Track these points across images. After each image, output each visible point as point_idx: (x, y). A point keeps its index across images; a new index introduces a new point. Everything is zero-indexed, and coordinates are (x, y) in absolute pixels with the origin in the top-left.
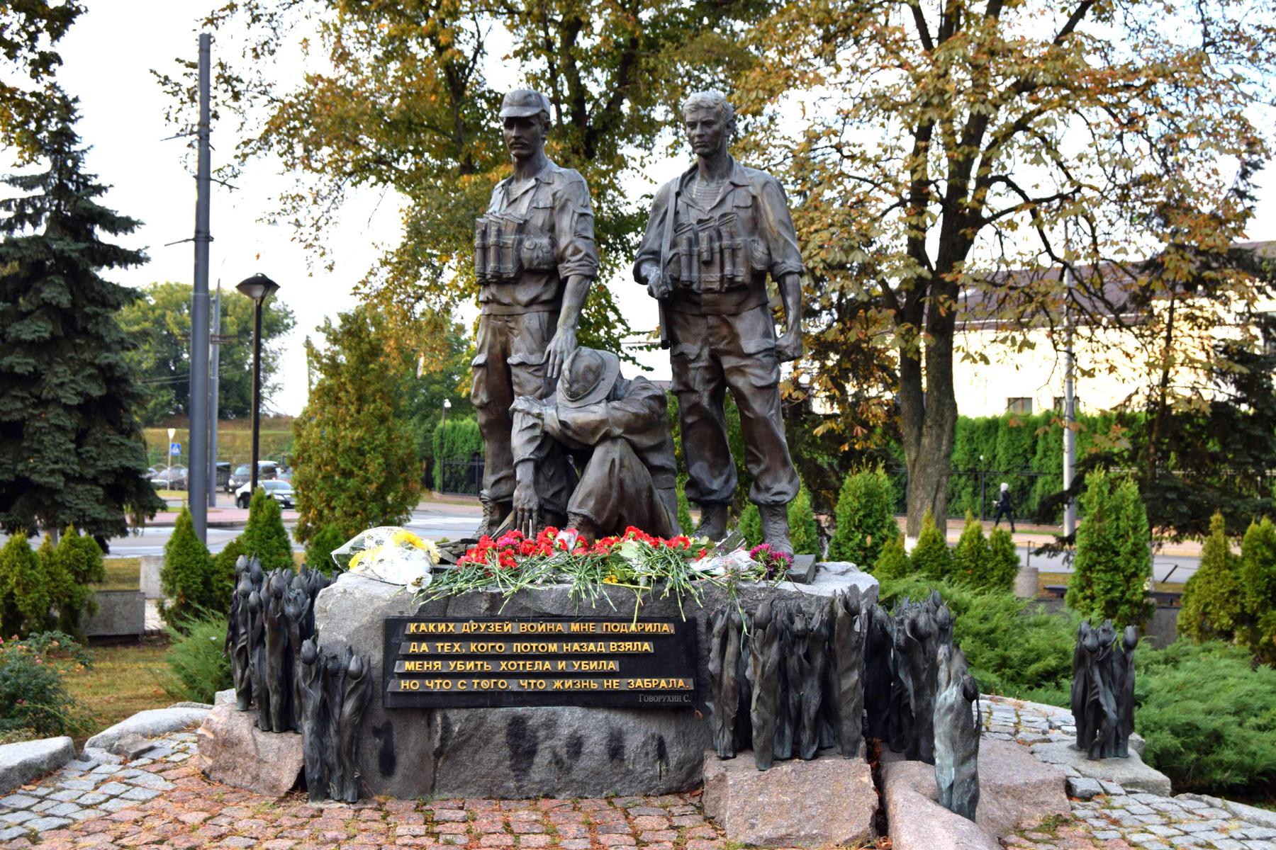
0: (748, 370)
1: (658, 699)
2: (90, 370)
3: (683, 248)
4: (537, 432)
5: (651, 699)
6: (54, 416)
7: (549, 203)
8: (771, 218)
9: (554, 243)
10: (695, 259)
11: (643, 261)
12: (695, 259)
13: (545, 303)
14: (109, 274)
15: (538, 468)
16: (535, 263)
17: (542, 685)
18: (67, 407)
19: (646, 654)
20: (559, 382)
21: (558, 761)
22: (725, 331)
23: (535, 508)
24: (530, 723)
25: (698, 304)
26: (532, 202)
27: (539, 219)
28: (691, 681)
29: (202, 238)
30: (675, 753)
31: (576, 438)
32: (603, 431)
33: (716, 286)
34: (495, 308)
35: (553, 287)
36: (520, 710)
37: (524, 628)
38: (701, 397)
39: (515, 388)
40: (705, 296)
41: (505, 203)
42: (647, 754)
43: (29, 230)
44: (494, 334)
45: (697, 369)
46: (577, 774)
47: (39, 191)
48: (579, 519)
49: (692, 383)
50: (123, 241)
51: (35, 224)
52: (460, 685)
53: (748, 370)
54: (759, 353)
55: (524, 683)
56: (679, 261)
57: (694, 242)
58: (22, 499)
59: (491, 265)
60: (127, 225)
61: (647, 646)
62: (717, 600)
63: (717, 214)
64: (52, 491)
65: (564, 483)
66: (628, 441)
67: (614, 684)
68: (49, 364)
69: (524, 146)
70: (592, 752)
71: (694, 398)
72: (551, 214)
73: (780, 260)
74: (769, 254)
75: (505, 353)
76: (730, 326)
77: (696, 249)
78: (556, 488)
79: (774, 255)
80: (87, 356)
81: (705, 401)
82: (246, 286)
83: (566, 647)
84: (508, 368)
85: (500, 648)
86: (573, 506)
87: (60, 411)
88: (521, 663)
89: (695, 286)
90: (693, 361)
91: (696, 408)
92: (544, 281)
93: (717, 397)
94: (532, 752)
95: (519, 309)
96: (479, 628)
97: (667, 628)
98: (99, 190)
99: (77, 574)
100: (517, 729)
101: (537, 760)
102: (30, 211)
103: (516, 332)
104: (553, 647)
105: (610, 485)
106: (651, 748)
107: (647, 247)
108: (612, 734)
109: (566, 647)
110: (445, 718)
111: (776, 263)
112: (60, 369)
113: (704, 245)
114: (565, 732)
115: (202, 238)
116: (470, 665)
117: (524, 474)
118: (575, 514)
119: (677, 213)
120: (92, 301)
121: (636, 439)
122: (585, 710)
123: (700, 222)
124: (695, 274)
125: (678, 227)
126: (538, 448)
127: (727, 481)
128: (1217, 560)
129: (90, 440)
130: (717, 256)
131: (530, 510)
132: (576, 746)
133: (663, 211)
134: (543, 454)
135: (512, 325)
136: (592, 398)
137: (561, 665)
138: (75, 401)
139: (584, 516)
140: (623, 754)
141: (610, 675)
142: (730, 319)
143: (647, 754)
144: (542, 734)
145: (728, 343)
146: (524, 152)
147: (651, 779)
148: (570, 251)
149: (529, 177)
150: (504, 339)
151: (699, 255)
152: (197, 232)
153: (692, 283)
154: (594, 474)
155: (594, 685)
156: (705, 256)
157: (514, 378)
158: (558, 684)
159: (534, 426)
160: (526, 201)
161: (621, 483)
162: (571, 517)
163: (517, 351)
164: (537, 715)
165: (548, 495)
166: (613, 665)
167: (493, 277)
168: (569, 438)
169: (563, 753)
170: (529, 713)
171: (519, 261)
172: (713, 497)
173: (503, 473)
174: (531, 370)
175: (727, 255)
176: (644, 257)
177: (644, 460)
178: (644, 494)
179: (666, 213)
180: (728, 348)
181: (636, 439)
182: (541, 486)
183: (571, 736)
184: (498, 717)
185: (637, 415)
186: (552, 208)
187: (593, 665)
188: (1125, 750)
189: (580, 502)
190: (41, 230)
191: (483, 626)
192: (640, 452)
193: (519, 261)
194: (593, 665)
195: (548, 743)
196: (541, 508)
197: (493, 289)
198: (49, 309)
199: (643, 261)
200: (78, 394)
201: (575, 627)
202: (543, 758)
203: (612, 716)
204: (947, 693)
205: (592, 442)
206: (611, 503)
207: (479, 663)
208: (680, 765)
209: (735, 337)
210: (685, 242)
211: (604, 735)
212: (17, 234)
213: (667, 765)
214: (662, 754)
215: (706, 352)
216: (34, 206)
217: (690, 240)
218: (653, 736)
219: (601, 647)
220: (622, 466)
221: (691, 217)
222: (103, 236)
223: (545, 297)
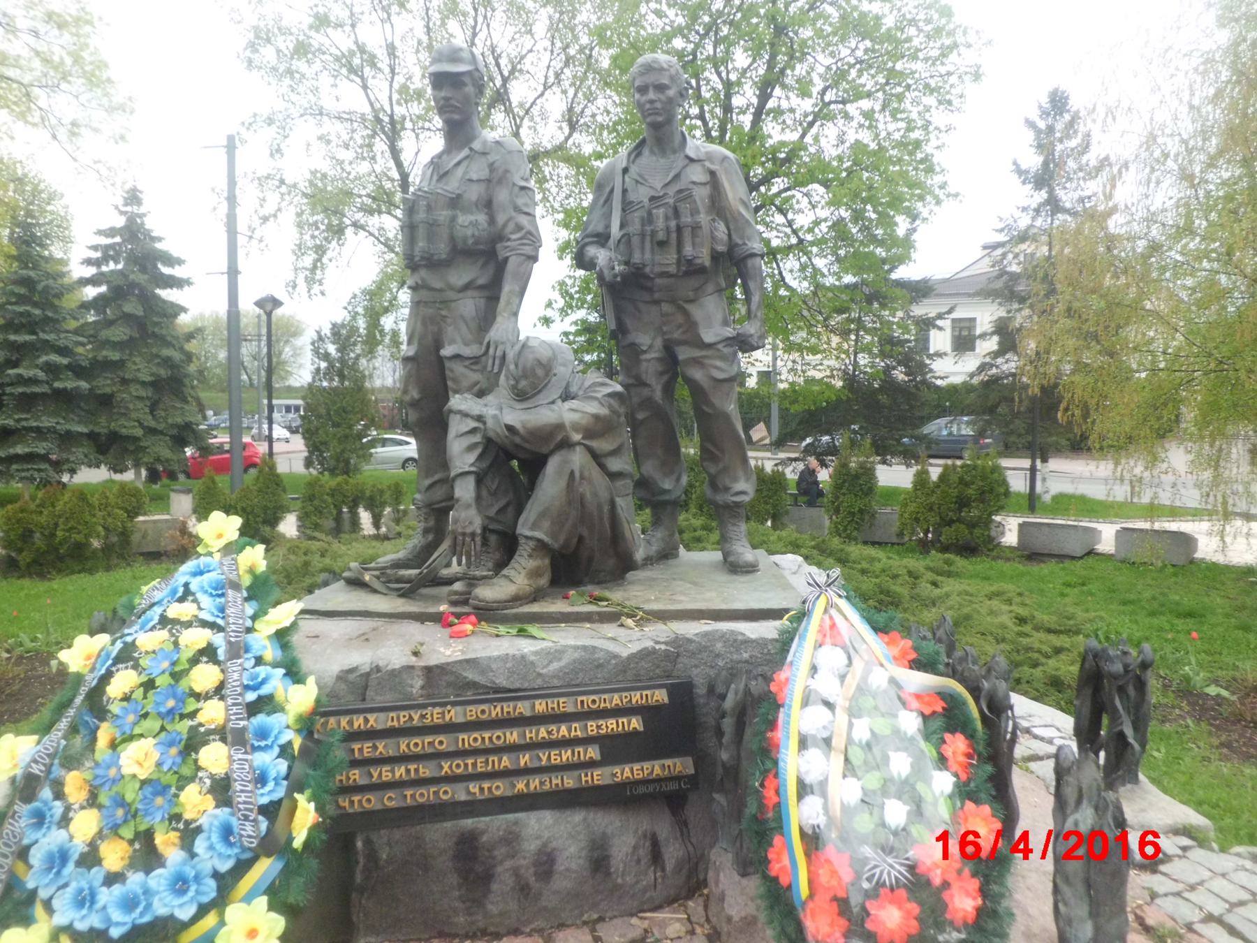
0: (707, 361)
1: (651, 788)
2: (157, 361)
3: (635, 227)
4: (477, 438)
5: (642, 790)
6: (135, 390)
7: (484, 174)
8: (730, 195)
9: (492, 221)
10: (648, 239)
11: (586, 244)
12: (648, 239)
13: (481, 287)
14: (166, 294)
15: (480, 481)
16: (470, 242)
17: (500, 788)
18: (143, 383)
19: (635, 732)
20: (502, 377)
21: (523, 889)
22: (680, 318)
23: (479, 531)
24: (485, 838)
25: (650, 290)
26: (465, 173)
27: (474, 193)
28: (689, 761)
29: (233, 273)
30: (673, 853)
31: (527, 446)
32: (559, 438)
33: (672, 269)
34: (425, 294)
35: (490, 270)
36: (469, 823)
37: (473, 713)
38: (653, 391)
39: (450, 383)
40: (658, 281)
41: (435, 178)
42: (639, 861)
43: (112, 266)
44: (424, 323)
45: (649, 361)
46: (549, 900)
47: (118, 239)
48: (532, 543)
49: (644, 377)
50: (177, 272)
51: (116, 262)
52: (390, 800)
53: (707, 361)
54: (719, 342)
55: (474, 787)
56: (629, 242)
57: (649, 219)
58: (114, 447)
59: (421, 244)
60: (179, 262)
61: (635, 723)
62: (718, 656)
63: (672, 191)
64: (136, 439)
65: (511, 496)
66: (585, 445)
67: (599, 777)
68: (131, 354)
69: (455, 109)
70: (567, 870)
71: (646, 392)
72: (488, 188)
73: (740, 242)
74: (729, 235)
75: (438, 344)
76: (686, 313)
77: (648, 228)
78: (502, 503)
79: (734, 237)
80: (154, 350)
81: (658, 395)
82: (259, 304)
83: (530, 734)
84: (441, 360)
85: (443, 742)
86: (523, 529)
87: (138, 386)
88: (470, 761)
89: (647, 270)
90: (645, 352)
91: (648, 403)
92: (480, 263)
93: (668, 389)
94: (486, 878)
95: (451, 295)
96: (411, 718)
97: (661, 696)
98: (160, 239)
99: (127, 511)
100: (468, 847)
101: (495, 887)
102: (111, 253)
103: (449, 320)
104: (513, 736)
105: (569, 503)
106: (644, 852)
107: (590, 230)
108: (593, 842)
109: (530, 734)
110: (368, 842)
111: (737, 245)
112: (138, 360)
113: (660, 223)
114: (531, 846)
115: (233, 273)
116: (400, 772)
117: (465, 490)
118: (527, 537)
119: (625, 191)
120: (158, 314)
121: (594, 444)
122: (557, 814)
123: (652, 199)
124: (648, 256)
125: (627, 206)
126: (480, 457)
127: (678, 479)
128: (921, 480)
129: (161, 406)
130: (674, 236)
131: (473, 535)
132: (546, 863)
133: (608, 189)
134: (484, 465)
135: (444, 313)
136: (543, 398)
137: (525, 759)
138: (149, 379)
139: (539, 540)
140: (608, 867)
141: (592, 764)
142: (687, 306)
143: (639, 861)
144: (500, 852)
145: (684, 333)
146: (456, 117)
147: (645, 890)
148: (511, 226)
149: (461, 148)
150: (435, 329)
151: (653, 233)
152: (229, 268)
153: (645, 266)
154: (550, 487)
155: (569, 782)
156: (661, 236)
157: (447, 372)
158: (520, 786)
159: (473, 431)
160: (460, 172)
161: (582, 497)
162: (522, 541)
163: (453, 342)
164: (492, 825)
165: (492, 512)
166: (593, 752)
167: (422, 258)
168: (517, 446)
169: (529, 875)
170: (482, 826)
171: (452, 239)
172: (667, 497)
173: (437, 477)
174: (467, 363)
175: (687, 233)
176: (587, 240)
177: (602, 466)
178: (606, 508)
179: (612, 191)
180: (684, 337)
181: (594, 444)
182: (484, 503)
183: (540, 852)
184: (440, 834)
185: (596, 417)
186: (489, 181)
187: (567, 755)
188: (1137, 776)
189: (531, 526)
190: (120, 266)
191: (416, 717)
192: (596, 456)
193: (452, 239)
194: (567, 755)
195: (508, 864)
196: (485, 529)
197: (423, 273)
198: (127, 317)
199: (586, 244)
200: (152, 375)
201: (540, 706)
202: (503, 882)
203: (592, 815)
204: (1077, 816)
205: (545, 450)
206: (570, 522)
207: (412, 767)
208: (678, 868)
209: (691, 325)
210: (637, 221)
211: (583, 844)
212: (104, 269)
213: (663, 870)
214: (656, 857)
215: (659, 343)
216: (115, 250)
217: (642, 219)
218: (645, 836)
219: (576, 730)
220: (582, 478)
221: (641, 195)
222: (166, 270)
223: (481, 282)
